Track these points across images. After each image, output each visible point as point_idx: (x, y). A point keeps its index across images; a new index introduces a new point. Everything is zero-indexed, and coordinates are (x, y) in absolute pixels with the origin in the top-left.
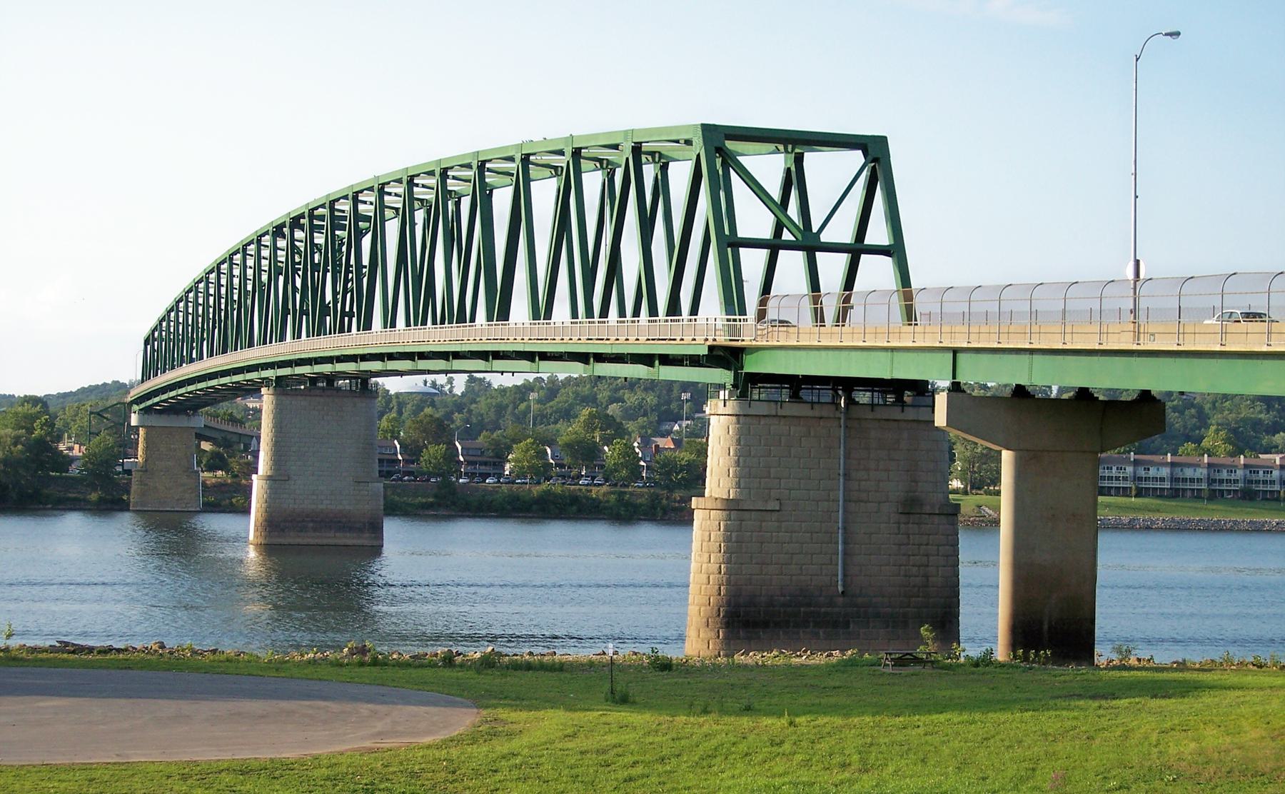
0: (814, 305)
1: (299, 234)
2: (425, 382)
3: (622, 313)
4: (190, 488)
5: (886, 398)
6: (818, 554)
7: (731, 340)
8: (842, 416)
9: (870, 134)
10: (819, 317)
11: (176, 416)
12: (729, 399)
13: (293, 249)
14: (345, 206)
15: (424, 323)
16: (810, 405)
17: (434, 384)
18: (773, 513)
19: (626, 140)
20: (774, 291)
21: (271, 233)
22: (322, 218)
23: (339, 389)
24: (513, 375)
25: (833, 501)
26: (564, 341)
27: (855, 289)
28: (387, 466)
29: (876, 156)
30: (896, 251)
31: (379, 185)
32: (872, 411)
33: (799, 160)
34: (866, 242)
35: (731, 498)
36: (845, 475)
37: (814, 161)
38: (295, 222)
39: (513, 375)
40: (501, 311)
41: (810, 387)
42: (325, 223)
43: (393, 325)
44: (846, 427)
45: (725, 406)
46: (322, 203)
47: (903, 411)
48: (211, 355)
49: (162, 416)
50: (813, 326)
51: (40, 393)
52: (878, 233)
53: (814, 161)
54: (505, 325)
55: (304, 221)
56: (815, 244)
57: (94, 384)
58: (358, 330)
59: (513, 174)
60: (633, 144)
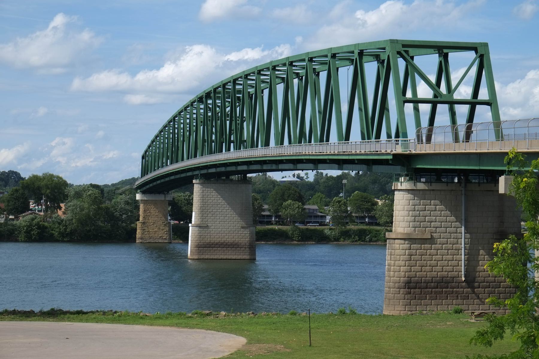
0: (497, 128)
1: (210, 101)
2: (294, 176)
3: (389, 136)
4: (166, 231)
5: (488, 179)
6: (451, 261)
7: (405, 151)
8: (463, 189)
9: (479, 42)
10: (456, 140)
11: (158, 195)
12: (404, 182)
13: (207, 108)
14: (230, 86)
15: (240, 149)
16: (446, 183)
17: (298, 177)
18: (427, 240)
19: (355, 49)
20: (475, 121)
21: (197, 101)
22: (219, 93)
23: (232, 180)
24: (313, 171)
25: (459, 233)
26: (327, 153)
27: (435, 125)
28: (267, 219)
29: (482, 53)
30: (491, 103)
31: (258, 71)
32: (479, 186)
33: (446, 56)
34: (478, 99)
35: (405, 232)
36: (465, 219)
37: (453, 56)
38: (208, 95)
39: (313, 171)
40: (324, 137)
41: (429, 174)
42: (221, 96)
43: (282, 143)
44: (465, 194)
45: (401, 185)
46: (229, 80)
47: (447, 186)
48: (171, 163)
49: (160, 195)
50: (496, 140)
51: (100, 183)
52: (484, 94)
53: (453, 56)
54: (268, 148)
55: (212, 95)
56: (451, 100)
57: (128, 179)
58: (226, 151)
59: (327, 63)
60: (359, 51)
